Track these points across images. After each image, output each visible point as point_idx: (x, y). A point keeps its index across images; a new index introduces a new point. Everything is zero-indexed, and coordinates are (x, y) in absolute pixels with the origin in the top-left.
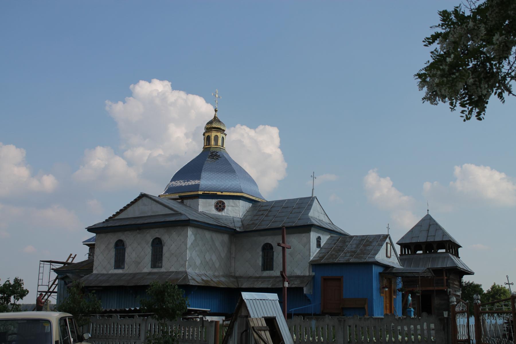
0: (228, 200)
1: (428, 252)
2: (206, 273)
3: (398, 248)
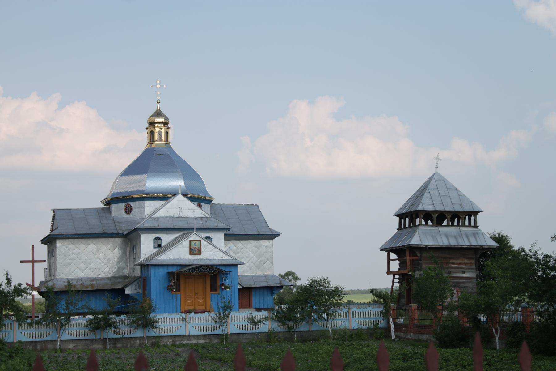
0: (135, 202)
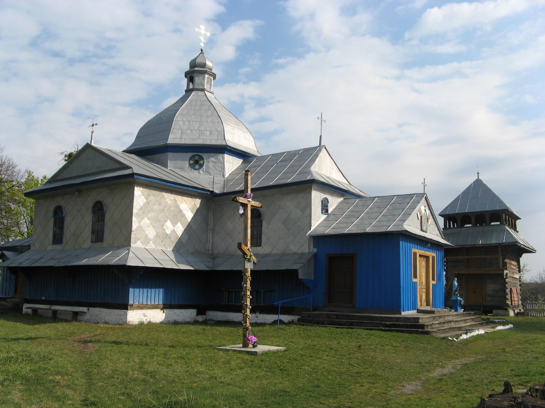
1: (478, 225)
2: (164, 249)
3: (441, 221)
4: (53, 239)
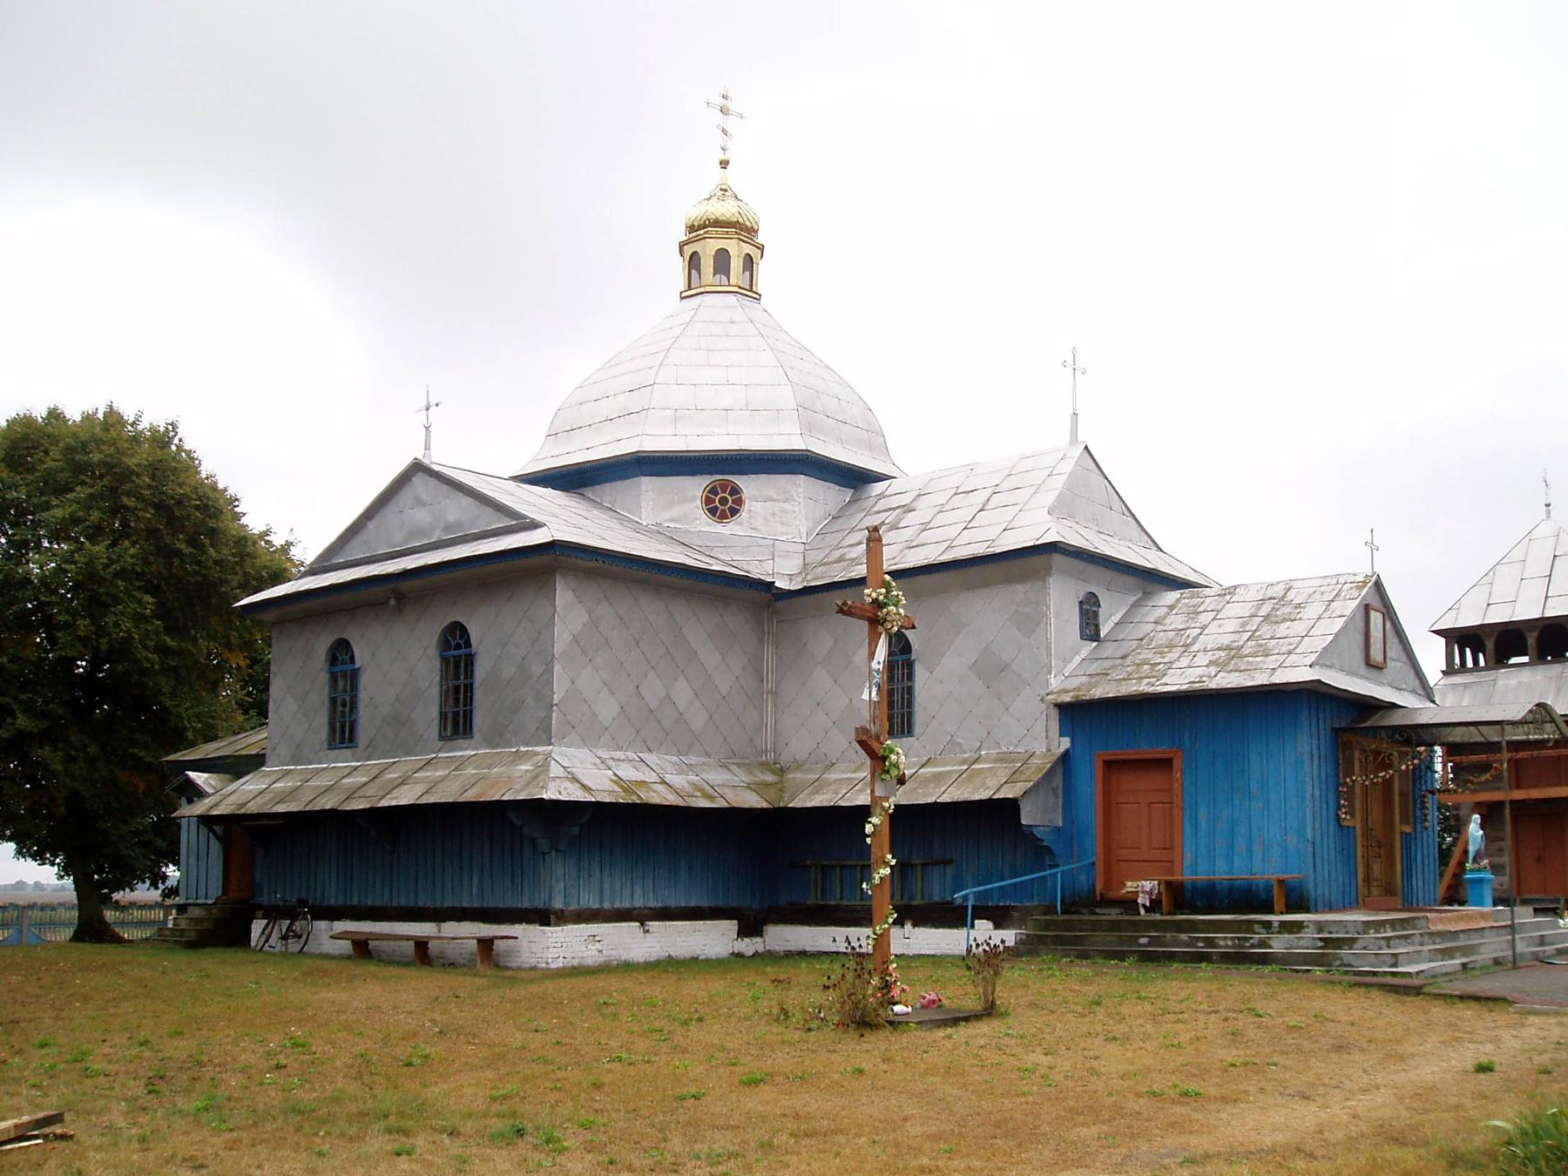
1: (1549, 658)
4: (330, 735)
